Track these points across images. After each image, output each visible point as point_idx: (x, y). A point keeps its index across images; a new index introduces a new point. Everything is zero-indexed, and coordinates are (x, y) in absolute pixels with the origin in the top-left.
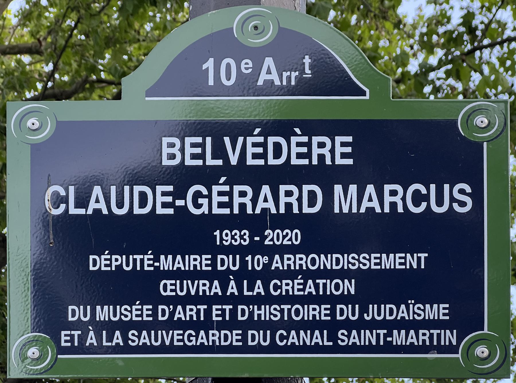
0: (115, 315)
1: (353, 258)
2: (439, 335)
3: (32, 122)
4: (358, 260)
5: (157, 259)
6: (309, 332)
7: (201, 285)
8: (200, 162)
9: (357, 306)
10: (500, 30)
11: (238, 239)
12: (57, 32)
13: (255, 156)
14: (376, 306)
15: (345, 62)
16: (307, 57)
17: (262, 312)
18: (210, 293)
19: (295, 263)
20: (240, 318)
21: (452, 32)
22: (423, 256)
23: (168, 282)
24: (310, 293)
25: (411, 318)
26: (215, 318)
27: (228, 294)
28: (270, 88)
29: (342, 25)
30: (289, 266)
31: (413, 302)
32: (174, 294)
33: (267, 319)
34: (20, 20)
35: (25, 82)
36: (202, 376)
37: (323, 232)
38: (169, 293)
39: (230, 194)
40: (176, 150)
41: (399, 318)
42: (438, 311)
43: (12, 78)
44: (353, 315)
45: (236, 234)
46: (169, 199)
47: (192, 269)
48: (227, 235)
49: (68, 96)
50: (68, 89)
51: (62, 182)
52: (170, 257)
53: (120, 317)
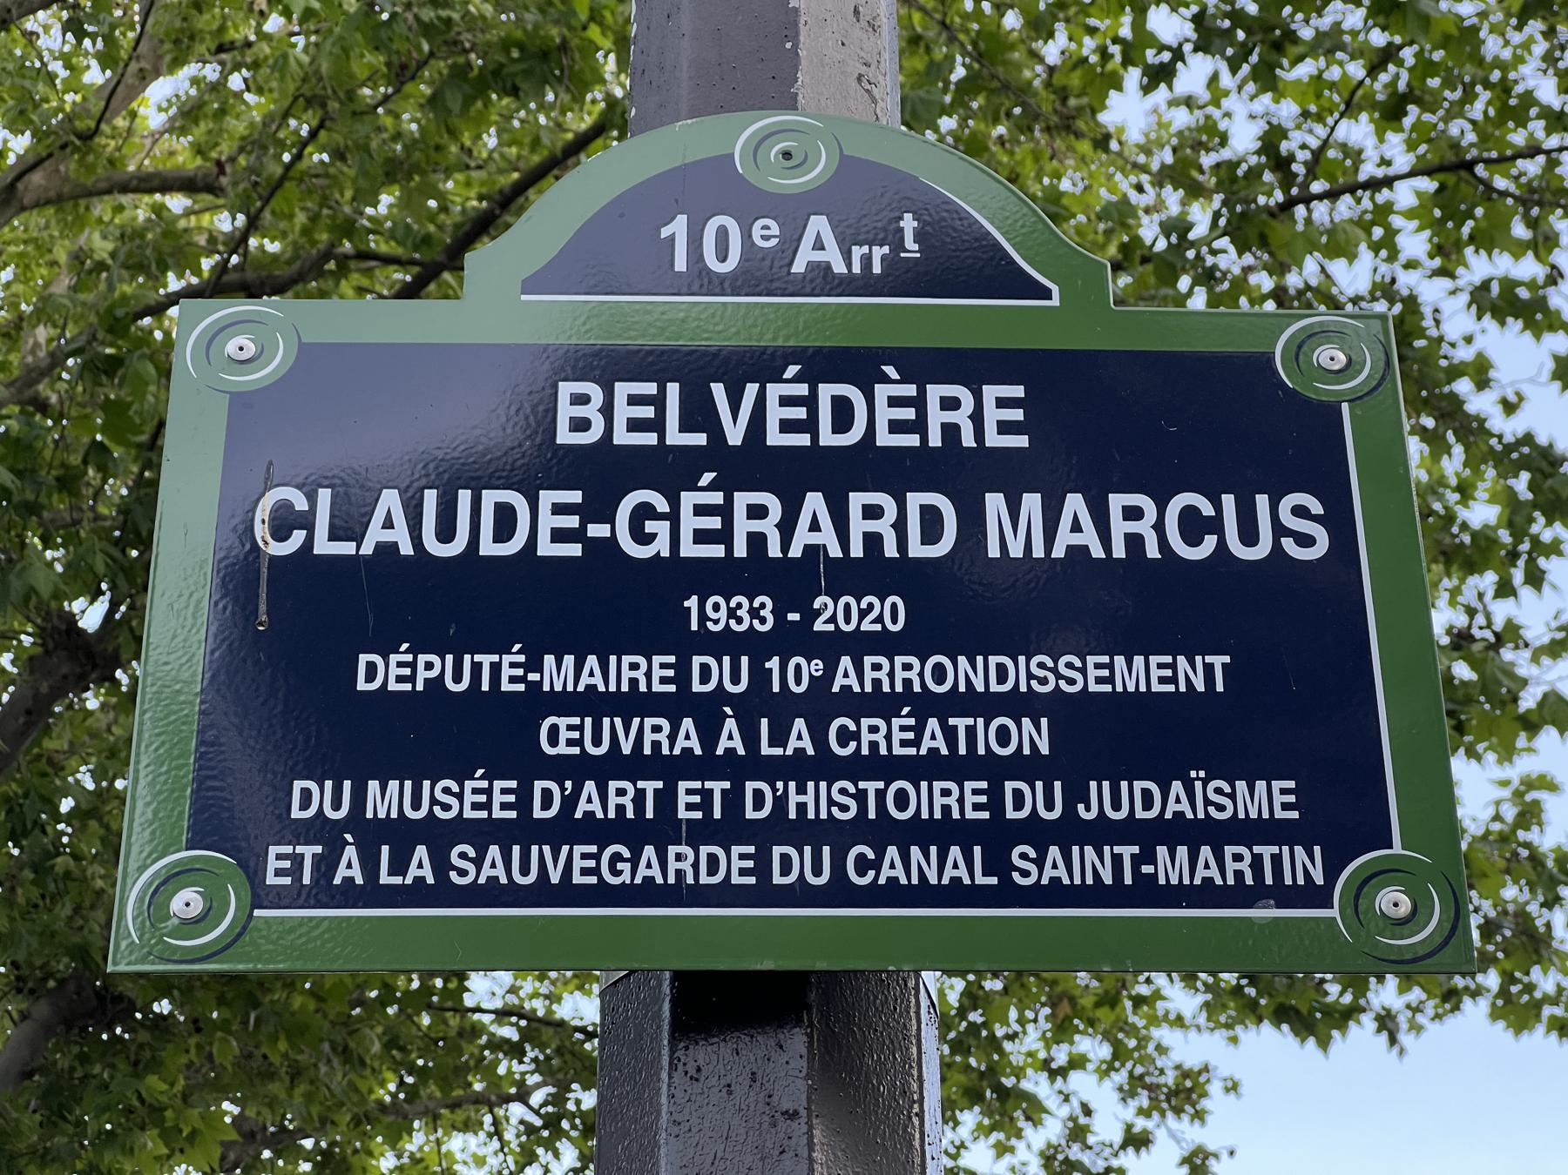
0: (416, 806)
1: (1041, 665)
2: (1277, 860)
3: (239, 344)
4: (1055, 671)
5: (534, 664)
6: (933, 849)
7: (647, 729)
8: (650, 439)
9: (1058, 785)
10: (1348, 162)
11: (747, 618)
12: (265, 148)
13: (787, 426)
14: (1106, 784)
15: (998, 228)
16: (908, 216)
17: (809, 799)
18: (671, 749)
19: (891, 675)
20: (750, 814)
21: (1233, 165)
22: (1219, 661)
23: (562, 722)
24: (934, 751)
25: (1201, 815)
26: (682, 814)
27: (720, 751)
28: (821, 279)
29: (973, 146)
30: (877, 683)
31: (1202, 774)
32: (576, 750)
33: (823, 815)
34: (172, 119)
35: (172, 255)
36: (646, 966)
37: (959, 605)
38: (562, 749)
39: (726, 511)
40: (591, 411)
41: (1168, 815)
42: (1270, 798)
43: (139, 247)
44: (1050, 806)
45: (739, 606)
46: (573, 522)
47: (625, 688)
48: (716, 607)
49: (279, 289)
50: (281, 272)
51: (300, 480)
52: (569, 660)
53: (431, 810)
